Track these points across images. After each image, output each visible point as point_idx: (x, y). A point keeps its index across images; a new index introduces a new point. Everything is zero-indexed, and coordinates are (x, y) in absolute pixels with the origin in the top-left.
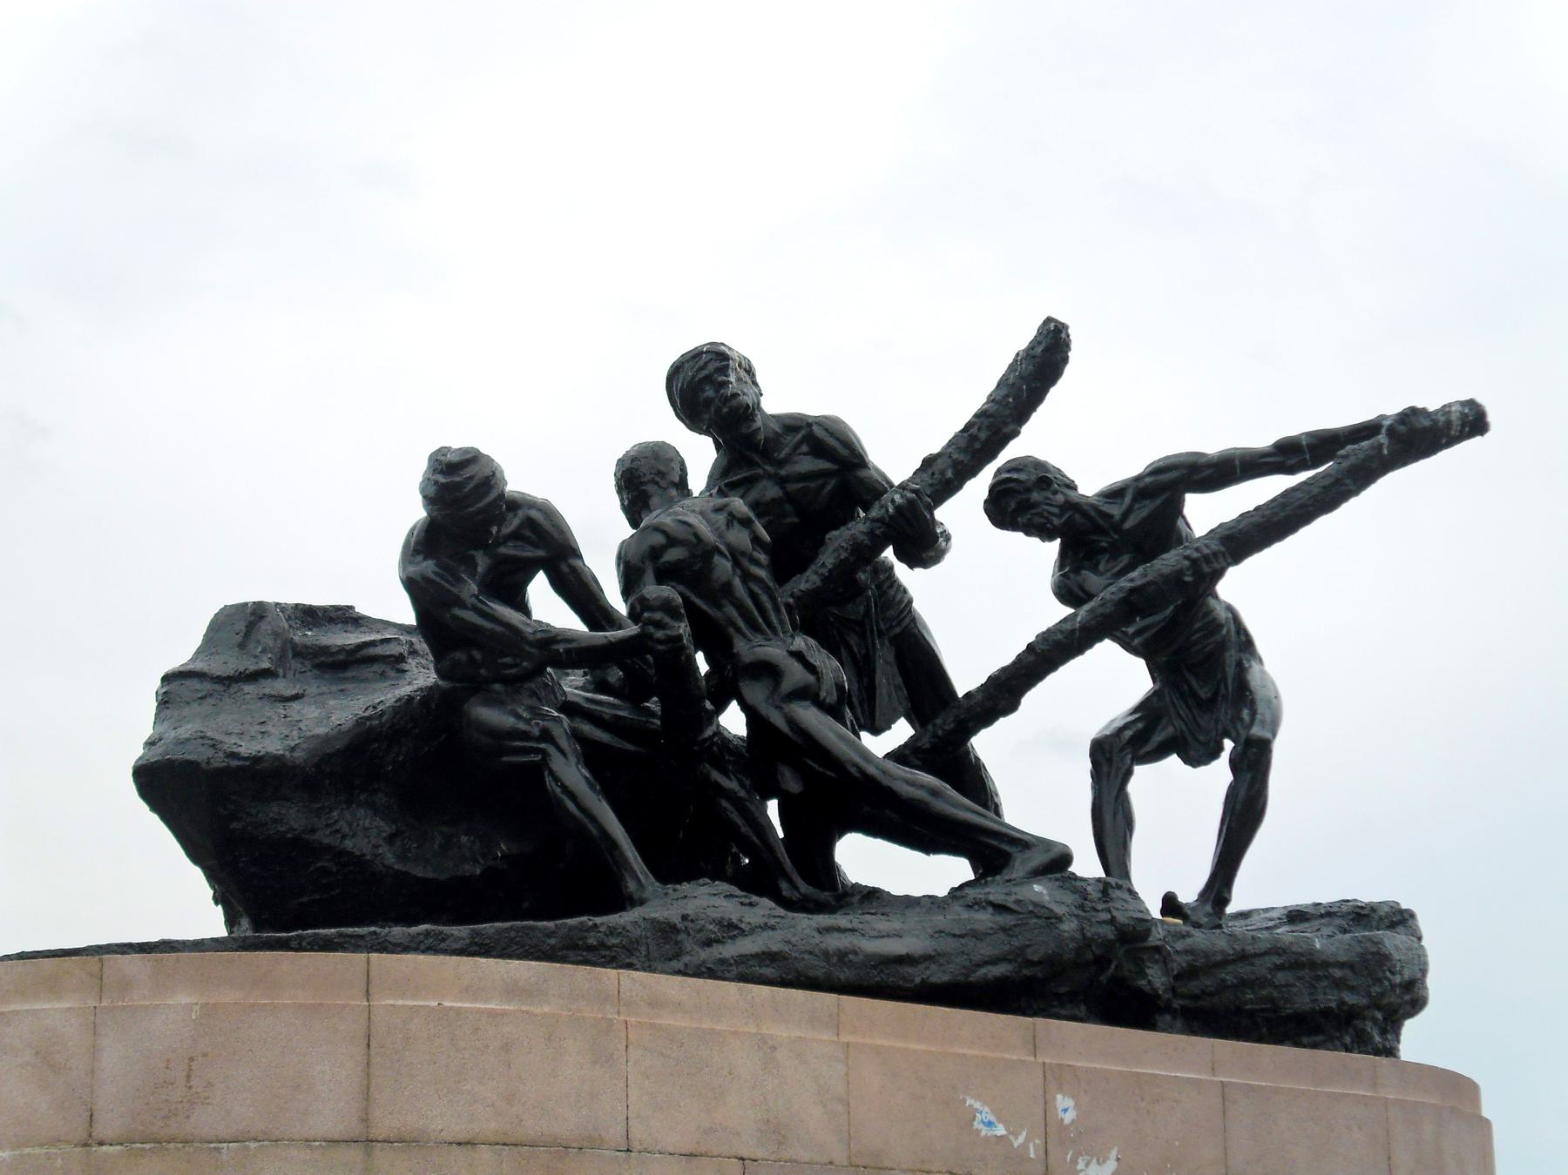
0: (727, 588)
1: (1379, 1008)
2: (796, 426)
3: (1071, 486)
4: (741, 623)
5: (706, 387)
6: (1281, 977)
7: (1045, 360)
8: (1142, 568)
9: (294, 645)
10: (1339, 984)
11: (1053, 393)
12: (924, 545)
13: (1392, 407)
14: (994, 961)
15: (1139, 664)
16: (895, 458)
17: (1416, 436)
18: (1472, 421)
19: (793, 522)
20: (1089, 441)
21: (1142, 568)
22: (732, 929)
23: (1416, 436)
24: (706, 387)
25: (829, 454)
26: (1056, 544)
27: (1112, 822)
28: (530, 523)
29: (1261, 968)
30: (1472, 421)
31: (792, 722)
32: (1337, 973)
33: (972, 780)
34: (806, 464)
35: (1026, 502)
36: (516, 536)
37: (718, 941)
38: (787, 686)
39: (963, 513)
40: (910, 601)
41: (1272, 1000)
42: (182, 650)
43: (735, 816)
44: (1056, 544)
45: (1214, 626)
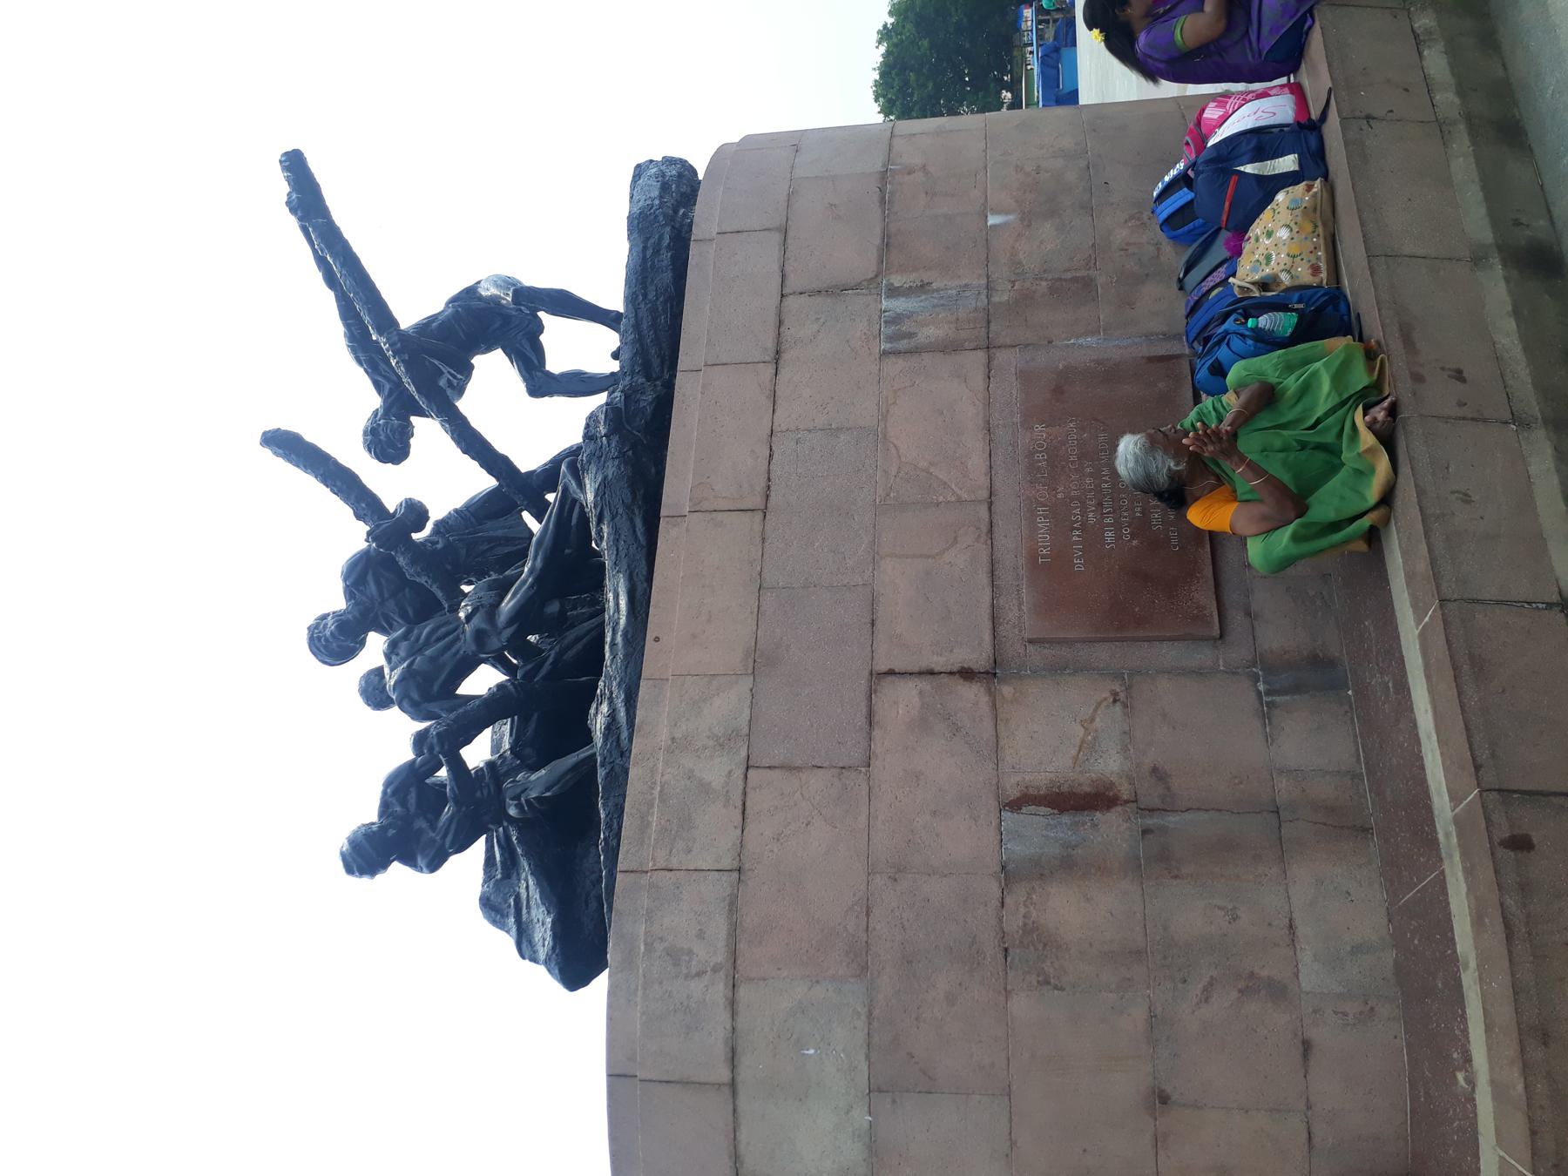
0: (433, 659)
1: (676, 211)
2: (350, 593)
3: (376, 413)
4: (453, 650)
5: (334, 642)
6: (651, 296)
7: (287, 445)
8: (419, 367)
9: (503, 878)
10: (657, 252)
11: (309, 438)
12: (415, 513)
13: (292, 223)
14: (632, 521)
15: (478, 361)
16: (354, 536)
17: (307, 201)
18: (295, 164)
19: (405, 589)
20: (342, 405)
21: (419, 367)
22: (612, 715)
23: (307, 201)
24: (334, 642)
25: (359, 574)
26: (414, 419)
27: (576, 384)
28: (394, 793)
29: (643, 312)
30: (295, 164)
31: (510, 622)
32: (649, 253)
33: (548, 476)
34: (372, 588)
35: (389, 442)
36: (404, 804)
37: (618, 738)
38: (485, 626)
39: (390, 485)
40: (456, 511)
41: (665, 302)
42: (505, 942)
43: (571, 653)
44: (414, 419)
45: (456, 316)
